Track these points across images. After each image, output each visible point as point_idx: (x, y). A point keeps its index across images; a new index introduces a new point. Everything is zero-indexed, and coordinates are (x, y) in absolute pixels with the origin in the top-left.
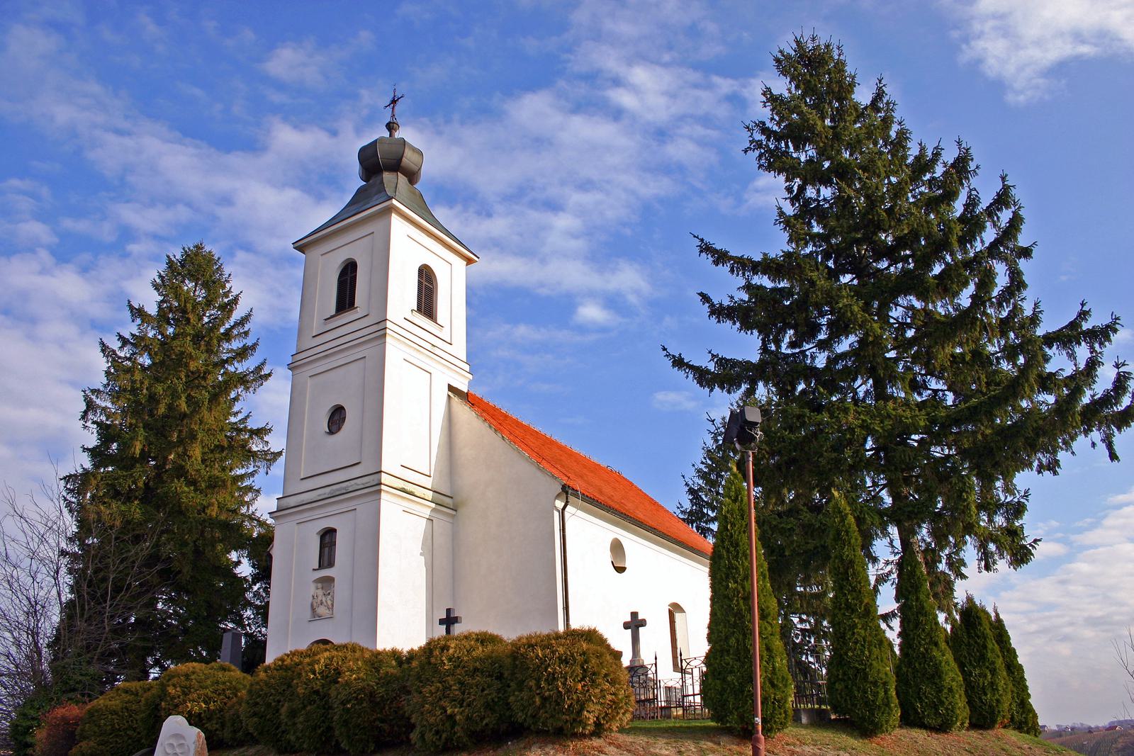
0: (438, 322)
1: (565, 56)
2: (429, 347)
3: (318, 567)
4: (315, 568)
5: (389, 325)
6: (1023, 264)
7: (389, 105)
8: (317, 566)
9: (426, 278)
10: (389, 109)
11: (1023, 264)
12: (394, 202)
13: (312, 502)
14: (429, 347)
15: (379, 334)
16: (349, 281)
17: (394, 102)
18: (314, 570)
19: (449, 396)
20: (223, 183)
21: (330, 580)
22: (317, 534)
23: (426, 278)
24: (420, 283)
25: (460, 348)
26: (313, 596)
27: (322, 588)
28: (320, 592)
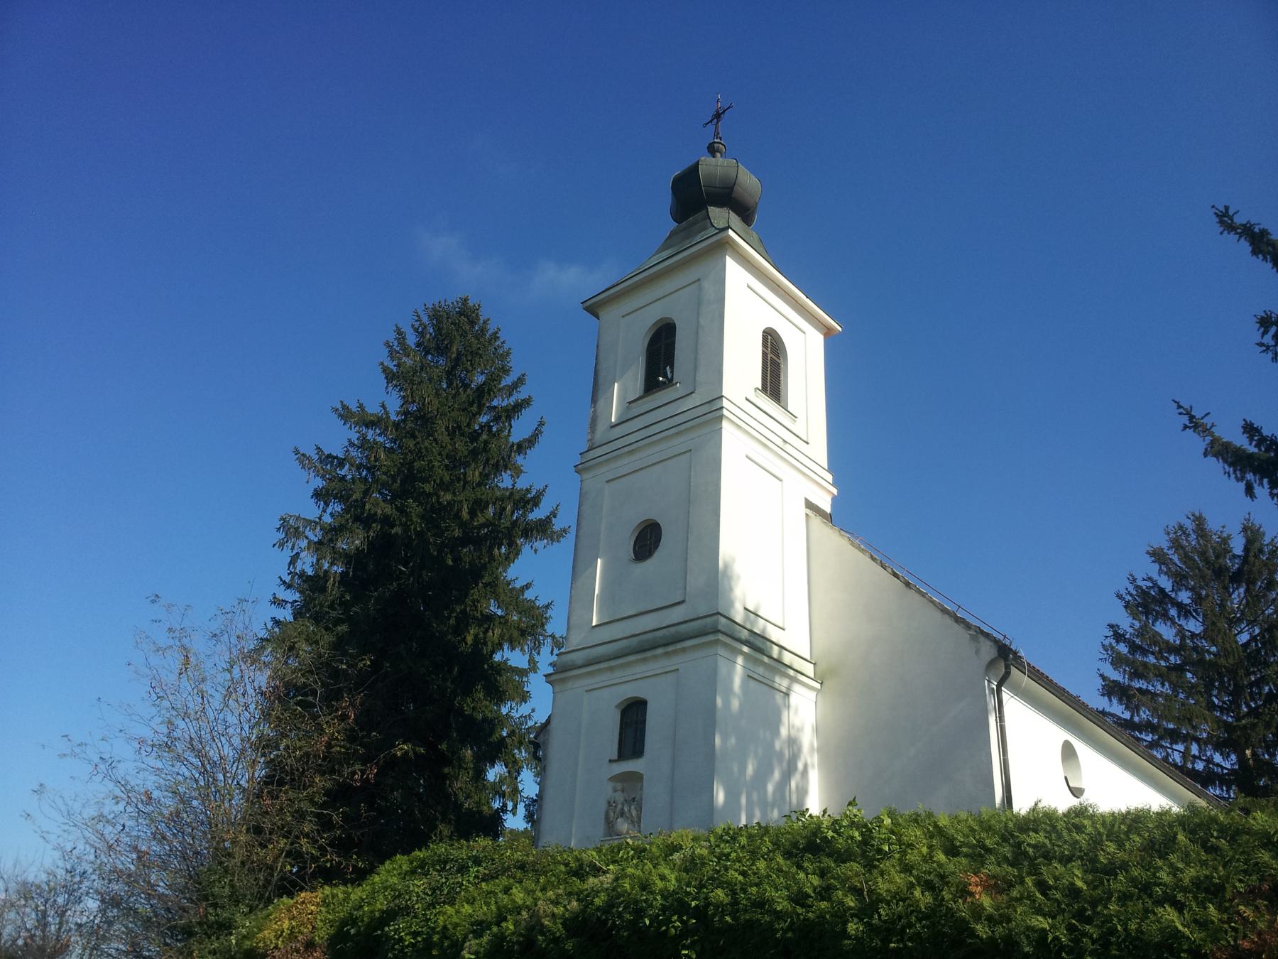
0: (789, 409)
1: (269, 732)
2: (780, 442)
3: (616, 758)
4: (613, 759)
5: (725, 403)
6: (1192, 429)
7: (711, 121)
8: (615, 757)
9: (773, 348)
10: (711, 127)
11: (1192, 429)
12: (731, 233)
13: (610, 685)
14: (780, 442)
15: (712, 413)
16: (284, 854)
17: (718, 116)
18: (610, 761)
19: (807, 514)
20: (717, 638)
21: (635, 778)
22: (617, 707)
23: (773, 348)
24: (764, 355)
25: (819, 449)
26: (609, 803)
27: (623, 791)
28: (620, 797)
